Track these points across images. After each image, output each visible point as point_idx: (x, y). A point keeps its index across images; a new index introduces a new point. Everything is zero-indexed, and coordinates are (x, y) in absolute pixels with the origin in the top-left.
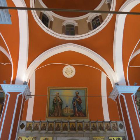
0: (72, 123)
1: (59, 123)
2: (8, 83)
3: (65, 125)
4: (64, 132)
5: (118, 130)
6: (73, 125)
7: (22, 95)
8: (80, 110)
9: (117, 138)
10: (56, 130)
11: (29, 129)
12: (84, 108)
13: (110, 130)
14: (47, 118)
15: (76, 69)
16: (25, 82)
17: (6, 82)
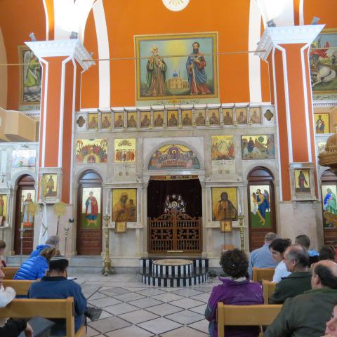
0: (172, 112)
1: (148, 114)
2: (41, 37)
3: (159, 116)
4: (157, 128)
5: (261, 123)
6: (173, 116)
7: (71, 61)
8: (201, 81)
9: (257, 137)
10: (142, 125)
11: (94, 125)
12: (209, 77)
13: (245, 122)
14: (138, 100)
15: (166, 9)
16: (73, 33)
17: (35, 35)
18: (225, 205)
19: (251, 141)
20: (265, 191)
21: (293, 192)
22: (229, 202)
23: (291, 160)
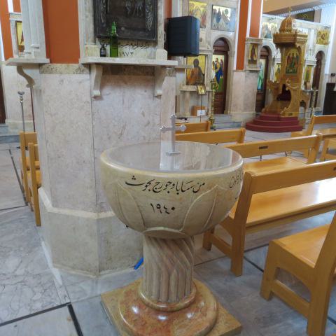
18: (196, 72)
19: (219, 12)
20: (222, 61)
21: (246, 62)
22: (200, 69)
23: (248, 35)
